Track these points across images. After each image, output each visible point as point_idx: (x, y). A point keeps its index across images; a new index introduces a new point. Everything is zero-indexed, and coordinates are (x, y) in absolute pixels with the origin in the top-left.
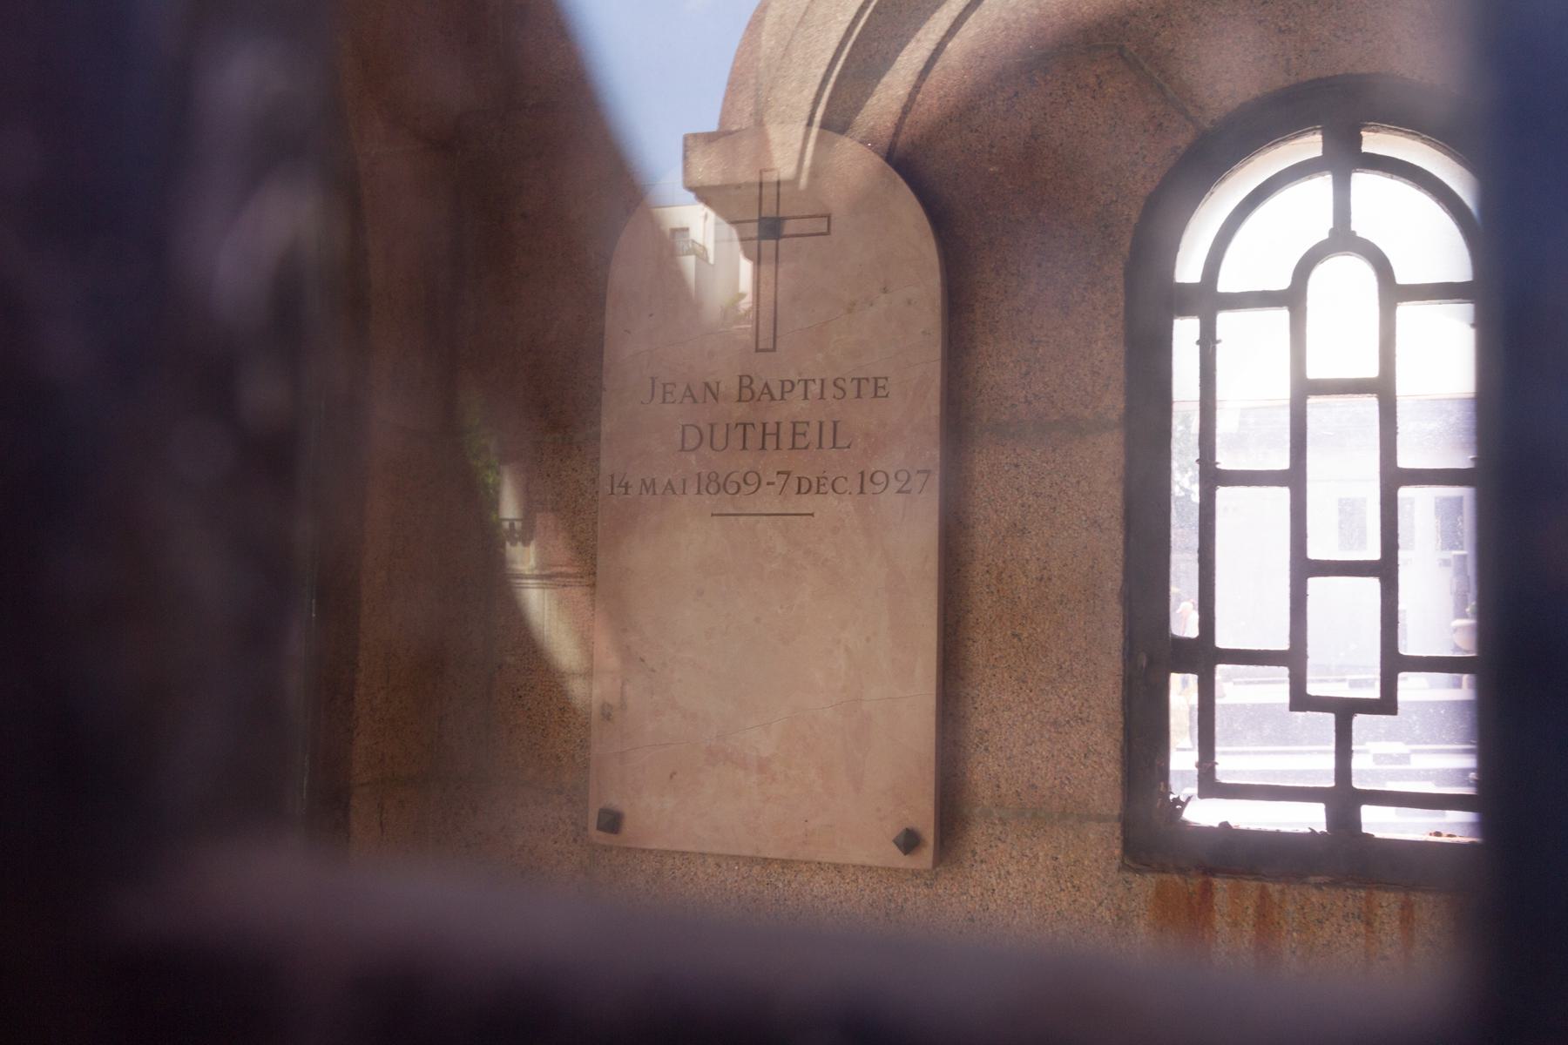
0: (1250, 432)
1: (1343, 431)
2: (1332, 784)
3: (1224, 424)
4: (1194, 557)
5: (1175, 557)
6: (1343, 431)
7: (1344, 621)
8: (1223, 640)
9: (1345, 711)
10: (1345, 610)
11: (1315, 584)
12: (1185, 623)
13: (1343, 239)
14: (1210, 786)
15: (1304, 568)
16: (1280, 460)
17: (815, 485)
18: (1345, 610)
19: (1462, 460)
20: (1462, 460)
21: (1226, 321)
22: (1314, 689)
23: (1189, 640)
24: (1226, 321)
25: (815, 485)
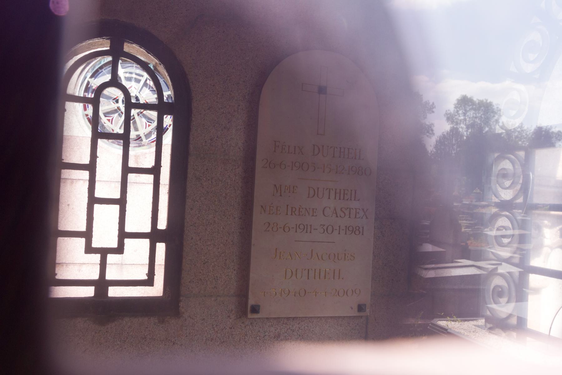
0: (141, 189)
1: (108, 187)
2: (125, 44)
3: (151, 188)
4: (161, 182)
5: (163, 262)
6: (108, 187)
7: (106, 221)
8: (146, 243)
9: (104, 252)
10: (105, 217)
11: (117, 196)
12: (161, 248)
13: (115, 82)
14: (149, 282)
15: (122, 202)
16: (131, 177)
17: (294, 273)
18: (105, 217)
19: (66, 174)
20: (66, 174)
21: (147, 229)
22: (115, 245)
23: (160, 242)
24: (147, 229)
25: (294, 273)
